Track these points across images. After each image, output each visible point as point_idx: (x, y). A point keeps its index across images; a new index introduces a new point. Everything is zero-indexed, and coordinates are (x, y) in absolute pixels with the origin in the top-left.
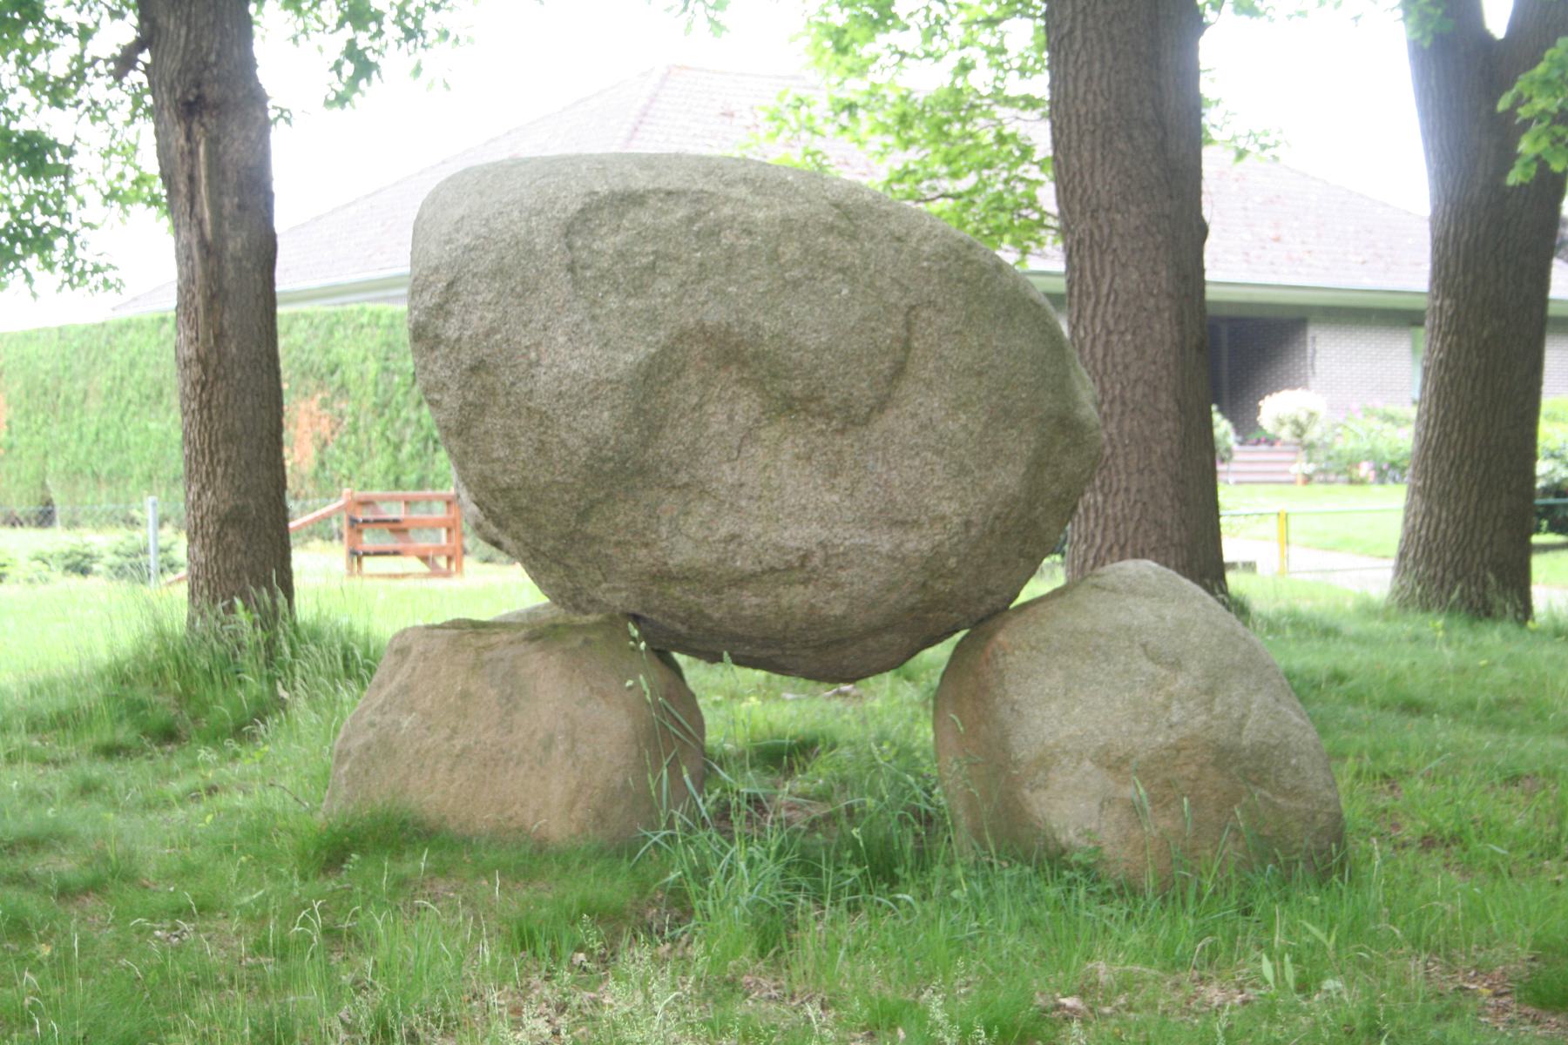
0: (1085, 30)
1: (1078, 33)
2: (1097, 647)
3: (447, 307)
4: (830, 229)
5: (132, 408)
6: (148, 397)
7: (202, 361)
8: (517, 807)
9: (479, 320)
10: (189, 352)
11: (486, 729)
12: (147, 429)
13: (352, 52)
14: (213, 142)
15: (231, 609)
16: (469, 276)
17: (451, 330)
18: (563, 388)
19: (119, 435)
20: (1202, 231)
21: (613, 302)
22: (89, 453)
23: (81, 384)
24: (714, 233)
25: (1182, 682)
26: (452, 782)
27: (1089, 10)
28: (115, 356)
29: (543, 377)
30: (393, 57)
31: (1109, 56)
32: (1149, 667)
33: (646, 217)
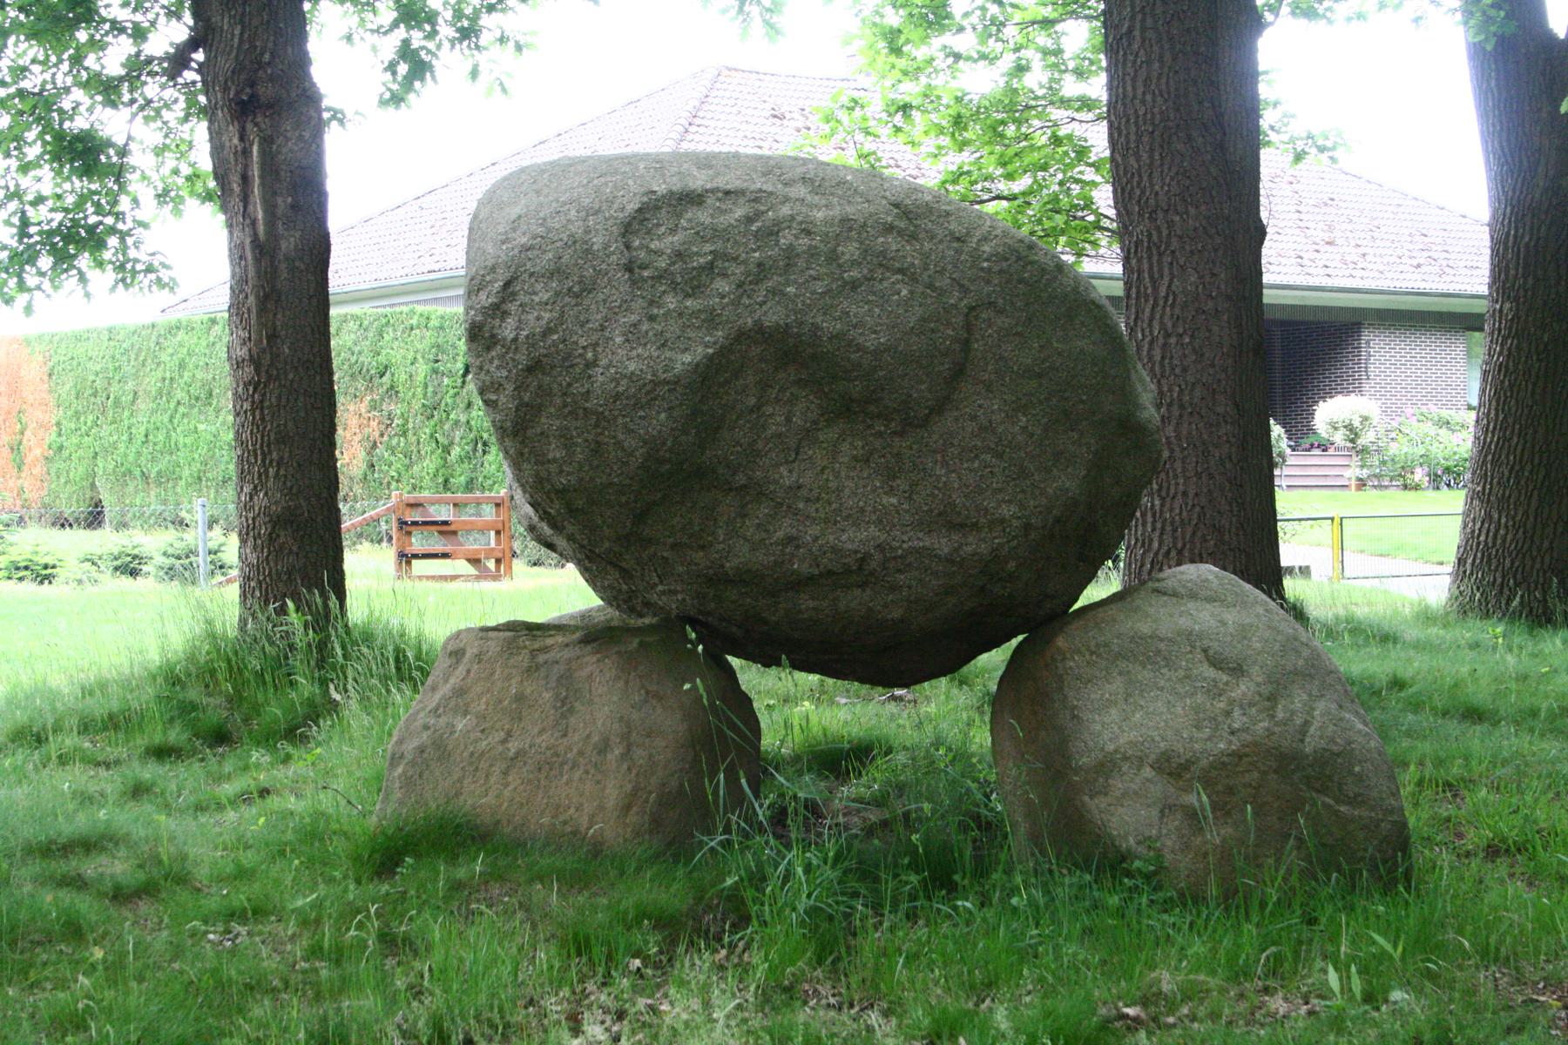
0: (1143, 30)
1: (1137, 33)
2: (1158, 652)
3: (504, 307)
4: (889, 229)
5: (182, 409)
6: (197, 399)
7: (255, 361)
8: (572, 811)
9: (535, 320)
10: (242, 352)
11: (540, 733)
12: (196, 430)
13: (406, 51)
14: (267, 142)
15: (282, 611)
16: (526, 276)
17: (508, 330)
18: (620, 389)
19: (168, 437)
20: (1260, 233)
21: (671, 302)
22: (139, 453)
23: (130, 385)
24: (773, 232)
25: (1243, 689)
26: (507, 785)
27: (1147, 10)
28: (164, 357)
29: (599, 377)
30: (450, 61)
31: (1168, 56)
32: (1211, 673)
33: (703, 216)
